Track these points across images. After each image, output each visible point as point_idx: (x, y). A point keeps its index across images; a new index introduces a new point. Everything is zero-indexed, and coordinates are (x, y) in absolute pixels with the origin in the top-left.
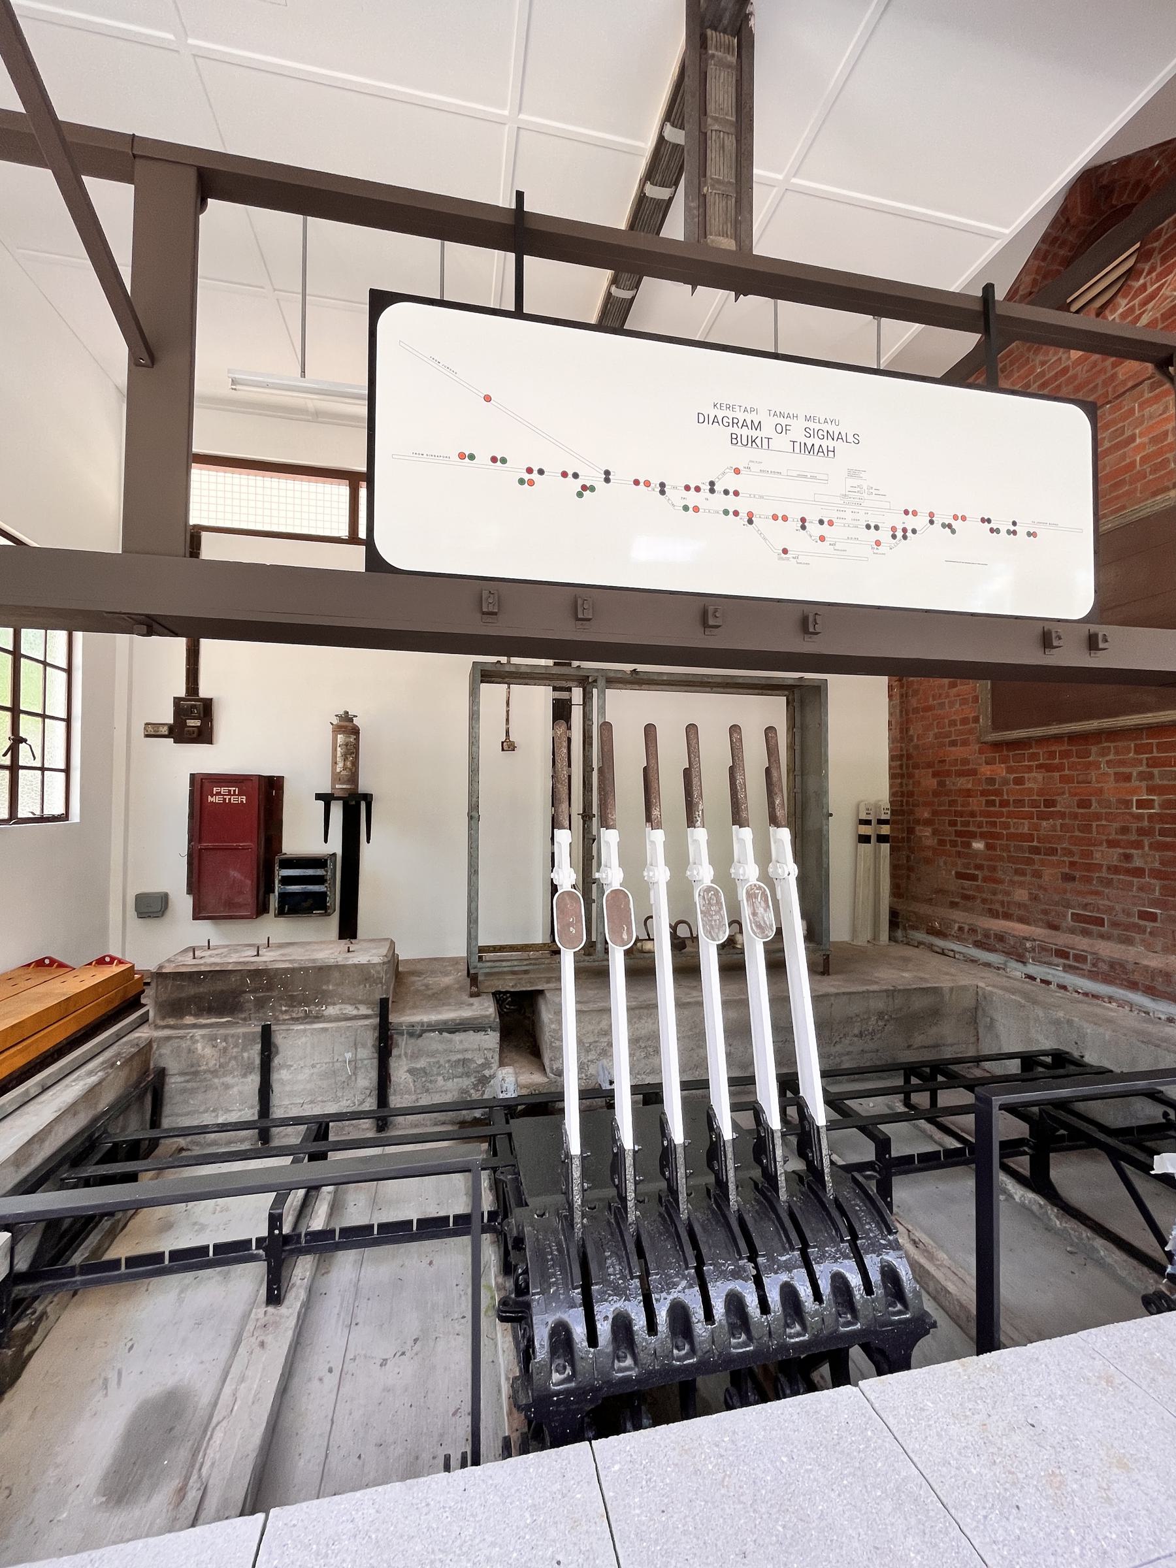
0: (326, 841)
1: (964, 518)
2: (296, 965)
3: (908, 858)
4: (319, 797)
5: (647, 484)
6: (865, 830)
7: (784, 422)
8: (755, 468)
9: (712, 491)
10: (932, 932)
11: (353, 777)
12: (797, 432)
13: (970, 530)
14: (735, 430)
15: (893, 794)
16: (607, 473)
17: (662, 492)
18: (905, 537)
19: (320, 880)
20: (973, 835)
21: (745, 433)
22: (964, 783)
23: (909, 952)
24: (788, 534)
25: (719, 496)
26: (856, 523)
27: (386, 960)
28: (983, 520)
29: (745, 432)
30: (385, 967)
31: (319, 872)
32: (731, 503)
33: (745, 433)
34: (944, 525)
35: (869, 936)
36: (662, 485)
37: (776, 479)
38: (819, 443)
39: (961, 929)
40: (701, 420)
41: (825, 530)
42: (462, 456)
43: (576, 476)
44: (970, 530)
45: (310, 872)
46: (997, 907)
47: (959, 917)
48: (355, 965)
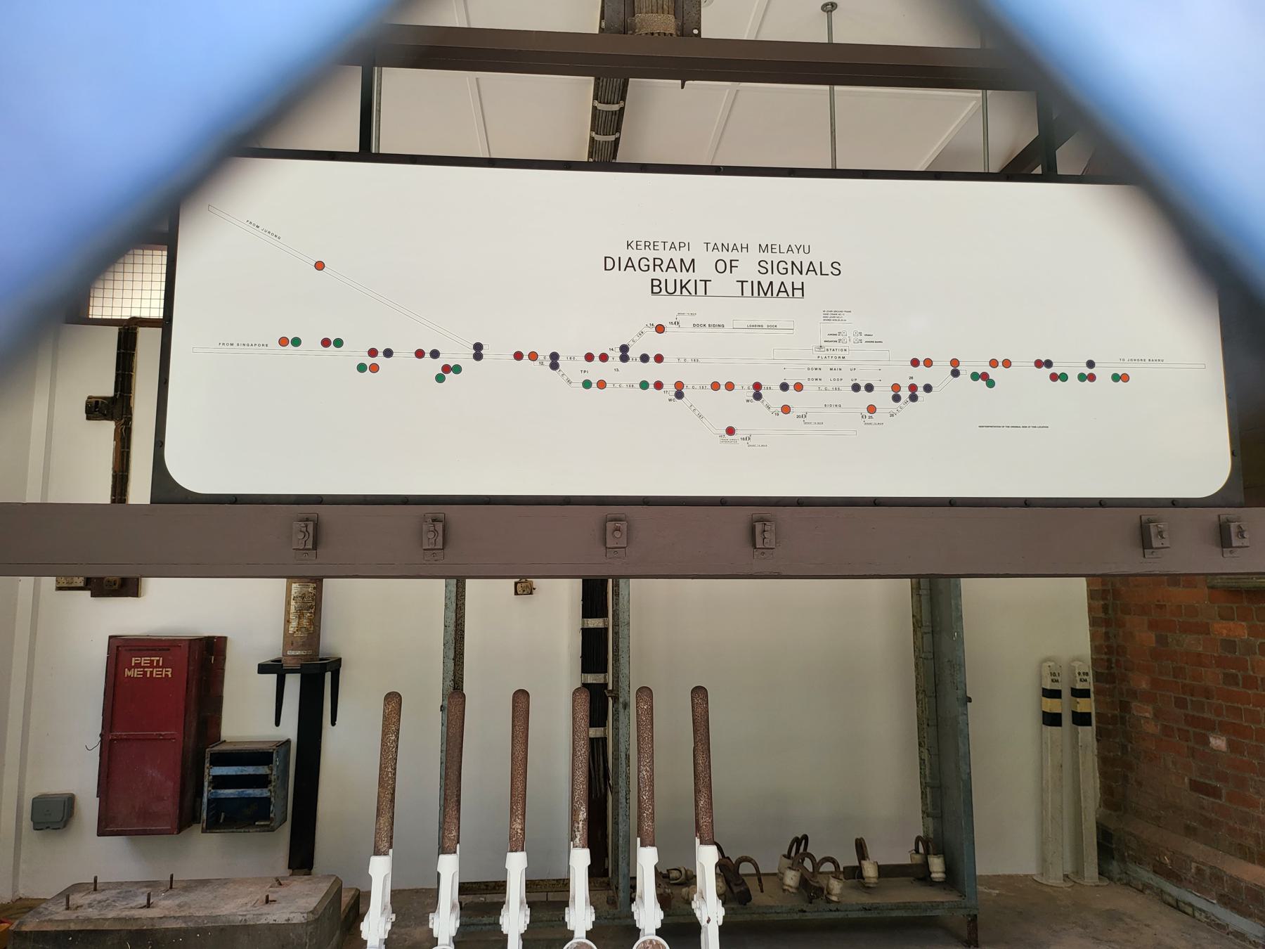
0: (277, 723)
1: (1007, 364)
2: (191, 925)
3: (1124, 747)
4: (263, 669)
5: (533, 356)
6: (1052, 705)
7: (727, 256)
8: (686, 322)
9: (624, 358)
10: (1160, 870)
11: (312, 634)
12: (748, 268)
13: (1022, 382)
14: (658, 274)
15: (1095, 649)
16: (478, 347)
17: (554, 366)
18: (914, 398)
19: (262, 781)
20: (1211, 727)
21: (670, 275)
22: (1191, 643)
23: (1125, 901)
24: (736, 406)
25: (634, 364)
26: (837, 384)
27: (311, 917)
28: (1039, 364)
29: (671, 276)
30: (310, 929)
31: (262, 770)
32: (651, 372)
33: (670, 275)
34: (975, 376)
35: (1069, 869)
36: (554, 356)
37: (722, 335)
38: (781, 278)
39: (1199, 870)
40: (609, 265)
41: (790, 397)
42: (283, 342)
43: (435, 354)
44: (1022, 382)
45: (250, 770)
46: (1250, 842)
47: (1196, 851)
48: (269, 927)
